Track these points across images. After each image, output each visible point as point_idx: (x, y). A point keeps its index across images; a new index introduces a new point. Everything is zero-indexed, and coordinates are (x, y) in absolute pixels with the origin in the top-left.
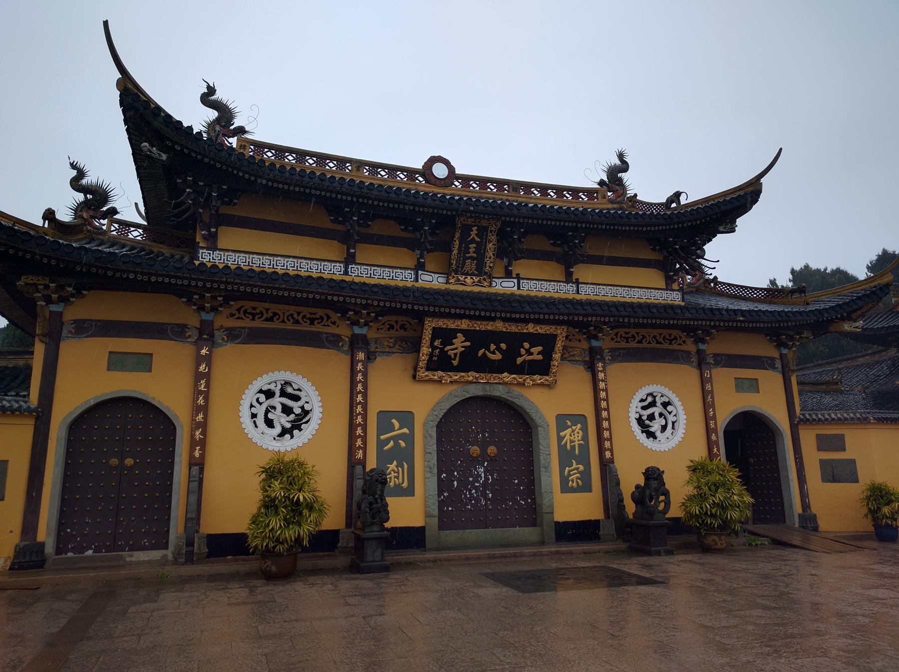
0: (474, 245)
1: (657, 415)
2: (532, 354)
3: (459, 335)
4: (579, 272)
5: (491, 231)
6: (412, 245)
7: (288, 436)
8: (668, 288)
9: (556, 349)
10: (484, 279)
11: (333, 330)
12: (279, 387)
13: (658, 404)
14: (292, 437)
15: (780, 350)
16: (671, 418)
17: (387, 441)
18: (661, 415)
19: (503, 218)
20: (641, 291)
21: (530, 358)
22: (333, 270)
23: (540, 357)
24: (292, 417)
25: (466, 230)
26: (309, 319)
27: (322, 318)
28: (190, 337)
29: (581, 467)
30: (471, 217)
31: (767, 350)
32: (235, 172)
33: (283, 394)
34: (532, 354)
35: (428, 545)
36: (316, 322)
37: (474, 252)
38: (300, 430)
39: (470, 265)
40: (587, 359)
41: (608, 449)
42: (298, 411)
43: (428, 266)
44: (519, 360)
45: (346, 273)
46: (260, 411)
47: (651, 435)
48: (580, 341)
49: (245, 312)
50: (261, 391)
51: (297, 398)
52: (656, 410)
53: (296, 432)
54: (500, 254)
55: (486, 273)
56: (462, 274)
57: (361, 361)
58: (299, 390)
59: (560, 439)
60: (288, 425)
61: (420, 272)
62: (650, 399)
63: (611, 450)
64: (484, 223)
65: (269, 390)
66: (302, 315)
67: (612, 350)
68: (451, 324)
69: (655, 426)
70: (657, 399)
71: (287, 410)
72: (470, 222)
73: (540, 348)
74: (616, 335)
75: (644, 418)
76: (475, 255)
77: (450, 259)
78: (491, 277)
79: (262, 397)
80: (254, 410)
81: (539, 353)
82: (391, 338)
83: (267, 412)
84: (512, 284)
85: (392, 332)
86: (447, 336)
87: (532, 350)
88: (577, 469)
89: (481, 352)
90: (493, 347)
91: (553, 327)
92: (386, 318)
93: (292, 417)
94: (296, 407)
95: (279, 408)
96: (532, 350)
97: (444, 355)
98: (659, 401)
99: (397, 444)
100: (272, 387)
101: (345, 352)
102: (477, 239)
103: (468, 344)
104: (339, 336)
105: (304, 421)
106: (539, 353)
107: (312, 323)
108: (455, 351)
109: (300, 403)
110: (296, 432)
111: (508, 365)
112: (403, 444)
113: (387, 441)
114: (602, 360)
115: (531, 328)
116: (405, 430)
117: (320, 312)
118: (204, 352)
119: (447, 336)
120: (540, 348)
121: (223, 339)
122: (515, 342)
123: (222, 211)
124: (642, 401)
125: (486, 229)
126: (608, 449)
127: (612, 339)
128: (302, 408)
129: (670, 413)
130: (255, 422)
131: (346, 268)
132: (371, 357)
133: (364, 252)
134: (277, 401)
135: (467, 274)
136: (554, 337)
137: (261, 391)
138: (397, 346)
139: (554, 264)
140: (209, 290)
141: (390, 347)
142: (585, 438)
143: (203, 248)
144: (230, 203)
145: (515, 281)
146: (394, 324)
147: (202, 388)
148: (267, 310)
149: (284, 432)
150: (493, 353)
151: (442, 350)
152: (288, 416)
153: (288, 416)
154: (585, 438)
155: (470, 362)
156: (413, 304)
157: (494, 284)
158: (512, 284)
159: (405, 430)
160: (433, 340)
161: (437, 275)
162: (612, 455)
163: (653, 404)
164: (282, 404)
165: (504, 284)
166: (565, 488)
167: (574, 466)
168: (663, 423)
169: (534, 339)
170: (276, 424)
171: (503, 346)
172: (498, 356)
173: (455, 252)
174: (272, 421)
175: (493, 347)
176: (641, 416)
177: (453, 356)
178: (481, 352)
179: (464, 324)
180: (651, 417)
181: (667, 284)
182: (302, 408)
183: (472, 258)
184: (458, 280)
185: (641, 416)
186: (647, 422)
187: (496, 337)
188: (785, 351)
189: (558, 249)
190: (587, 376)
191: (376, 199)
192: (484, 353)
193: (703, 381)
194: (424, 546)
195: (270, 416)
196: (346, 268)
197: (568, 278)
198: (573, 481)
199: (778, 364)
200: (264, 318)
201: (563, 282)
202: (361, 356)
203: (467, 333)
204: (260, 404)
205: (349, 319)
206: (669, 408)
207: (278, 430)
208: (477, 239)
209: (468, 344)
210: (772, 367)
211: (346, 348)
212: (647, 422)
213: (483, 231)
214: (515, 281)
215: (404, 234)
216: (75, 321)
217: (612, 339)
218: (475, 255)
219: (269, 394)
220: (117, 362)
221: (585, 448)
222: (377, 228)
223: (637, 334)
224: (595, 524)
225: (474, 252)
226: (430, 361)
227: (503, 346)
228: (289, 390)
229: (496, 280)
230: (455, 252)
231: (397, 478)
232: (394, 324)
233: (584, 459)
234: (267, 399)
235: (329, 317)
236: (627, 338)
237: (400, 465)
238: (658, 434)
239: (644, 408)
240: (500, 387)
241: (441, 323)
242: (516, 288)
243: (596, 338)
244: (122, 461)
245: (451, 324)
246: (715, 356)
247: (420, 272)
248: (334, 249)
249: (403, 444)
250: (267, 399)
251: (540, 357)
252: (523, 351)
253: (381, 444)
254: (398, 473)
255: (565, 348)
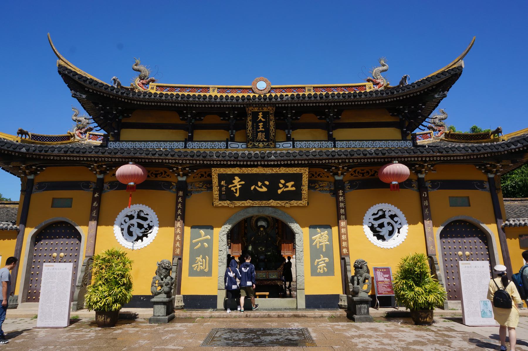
0: (262, 124)
1: (385, 224)
2: (288, 187)
3: (236, 178)
4: (338, 134)
5: (271, 114)
6: (226, 128)
7: (140, 241)
8: (404, 138)
9: (303, 183)
10: (271, 144)
11: (168, 179)
12: (137, 213)
13: (387, 216)
14: (142, 241)
15: (417, 175)
16: (396, 226)
17: (197, 243)
18: (389, 224)
19: (277, 105)
20: (382, 143)
21: (287, 189)
22: (179, 146)
23: (294, 189)
24: (143, 230)
25: (255, 115)
26: (155, 174)
27: (162, 173)
28: (91, 188)
29: (327, 259)
30: (256, 106)
31: (477, 175)
32: (120, 99)
33: (139, 217)
34: (288, 187)
35: (218, 308)
36: (365, 174)
37: (262, 128)
38: (147, 237)
39: (261, 136)
40: (332, 188)
41: (345, 248)
42: (146, 226)
43: (237, 139)
44: (279, 191)
45: (185, 147)
46: (126, 227)
47: (381, 237)
48: (328, 177)
49: (358, 172)
50: (127, 216)
51: (145, 219)
52: (387, 220)
53: (144, 238)
54: (278, 127)
55: (271, 140)
56: (257, 141)
57: (181, 196)
58: (147, 214)
59: (312, 241)
60: (141, 235)
61: (229, 143)
62: (380, 213)
63: (347, 248)
64: (265, 110)
65: (131, 215)
66: (151, 172)
67: (351, 182)
68: (229, 171)
69: (384, 232)
70: (386, 213)
71: (140, 226)
72: (256, 110)
73: (293, 183)
74: (355, 171)
75: (376, 226)
76: (263, 129)
77: (247, 133)
78: (275, 142)
79: (127, 219)
80: (122, 227)
81: (292, 186)
82: (201, 182)
83: (129, 227)
84: (289, 145)
85: (203, 178)
86: (230, 178)
87: (287, 184)
88: (324, 261)
89: (252, 188)
90: (260, 184)
91: (298, 169)
92: (199, 170)
93: (143, 230)
94: (145, 224)
95: (136, 225)
96: (287, 184)
97: (228, 190)
98: (387, 214)
99: (203, 245)
100: (133, 213)
101: (174, 192)
102: (263, 120)
103: (243, 183)
104: (171, 182)
105: (150, 232)
106: (292, 186)
107: (363, 176)
108: (236, 188)
109: (147, 222)
110: (144, 238)
111: (272, 194)
112: (206, 245)
113: (197, 243)
114: (343, 189)
115: (283, 170)
116: (209, 237)
117: (161, 170)
118: (96, 195)
119: (230, 178)
120: (293, 183)
121: (108, 188)
122: (274, 179)
123: (123, 121)
124: (374, 214)
125: (268, 113)
126: (345, 248)
127: (352, 175)
128: (149, 224)
129: (396, 222)
130: (122, 233)
131: (186, 144)
132: (187, 194)
133: (199, 134)
134: (135, 221)
135: (260, 141)
136: (301, 175)
137: (127, 216)
138: (204, 186)
139: (320, 130)
140: (181, 164)
141: (200, 188)
142: (330, 240)
143: (111, 141)
144: (128, 117)
145: (291, 143)
146: (204, 174)
147: (94, 215)
148: (371, 170)
149: (139, 238)
150: (261, 187)
151: (227, 187)
152: (141, 229)
153: (141, 229)
154: (330, 240)
155: (246, 193)
156: (203, 161)
157: (278, 146)
158: (289, 145)
159: (209, 237)
160: (220, 182)
161: (241, 144)
162: (348, 251)
163: (383, 216)
164: (138, 223)
165: (284, 146)
166: (314, 272)
167: (322, 259)
168: (390, 228)
169: (288, 177)
170: (134, 234)
171: (267, 183)
172: (264, 189)
173: (250, 128)
174: (132, 232)
175: (260, 184)
176: (373, 225)
177: (235, 191)
178: (252, 188)
179: (237, 171)
180: (381, 226)
181: (402, 136)
182: (149, 224)
183: (262, 131)
184: (254, 145)
185: (373, 225)
186: (378, 229)
187: (262, 177)
188: (491, 176)
189: (323, 121)
190: (333, 200)
191: (197, 104)
192: (255, 188)
193: (422, 199)
194: (216, 307)
195: (131, 229)
196: (186, 144)
197: (331, 138)
198: (320, 269)
199: (487, 185)
200: (370, 175)
201: (325, 141)
202: (181, 193)
203: (242, 177)
204: (126, 223)
205: (331, 172)
206: (396, 219)
207: (135, 237)
208: (263, 120)
209: (243, 183)
210: (482, 187)
211: (174, 190)
212: (378, 229)
213: (265, 115)
214: (291, 143)
215: (224, 122)
216: (110, 182)
217: (352, 175)
218: (263, 129)
219: (131, 217)
220: (55, 203)
221: (330, 248)
222: (208, 119)
223: (371, 170)
224: (336, 297)
225: (262, 128)
226: (220, 195)
227: (267, 183)
228: (142, 215)
229: (280, 143)
230: (250, 128)
231: (202, 265)
232: (315, 174)
233: (329, 252)
234: (130, 220)
235: (165, 172)
236: (363, 174)
237: (204, 258)
238: (386, 236)
239: (375, 219)
240: (270, 208)
241: (222, 171)
242: (291, 147)
243: (421, 172)
244: (58, 255)
245: (229, 171)
246: (433, 182)
247: (229, 143)
248: (181, 134)
249: (206, 245)
250: (130, 220)
251: (294, 189)
252: (281, 186)
253: (192, 245)
254: (202, 262)
255: (310, 182)
